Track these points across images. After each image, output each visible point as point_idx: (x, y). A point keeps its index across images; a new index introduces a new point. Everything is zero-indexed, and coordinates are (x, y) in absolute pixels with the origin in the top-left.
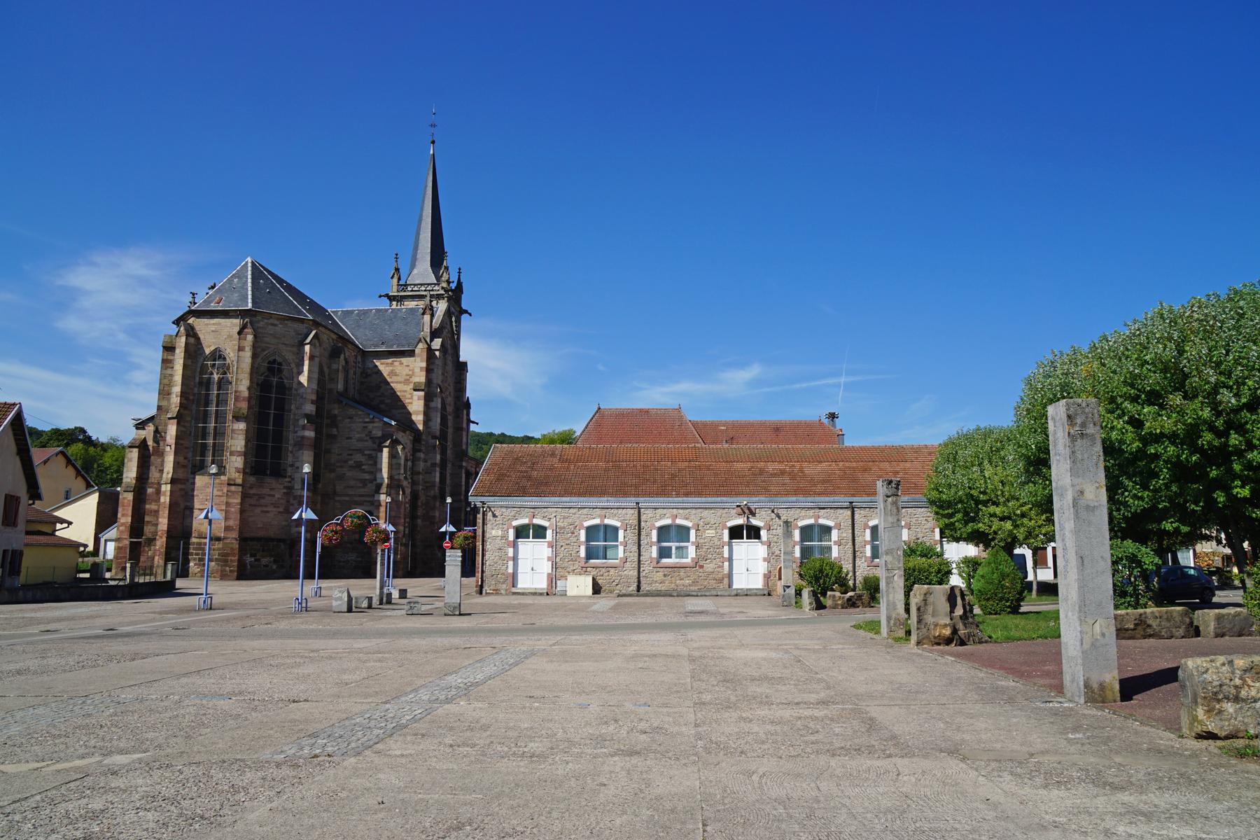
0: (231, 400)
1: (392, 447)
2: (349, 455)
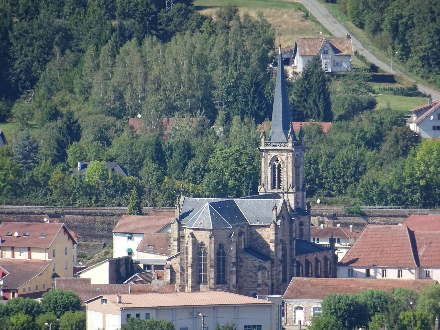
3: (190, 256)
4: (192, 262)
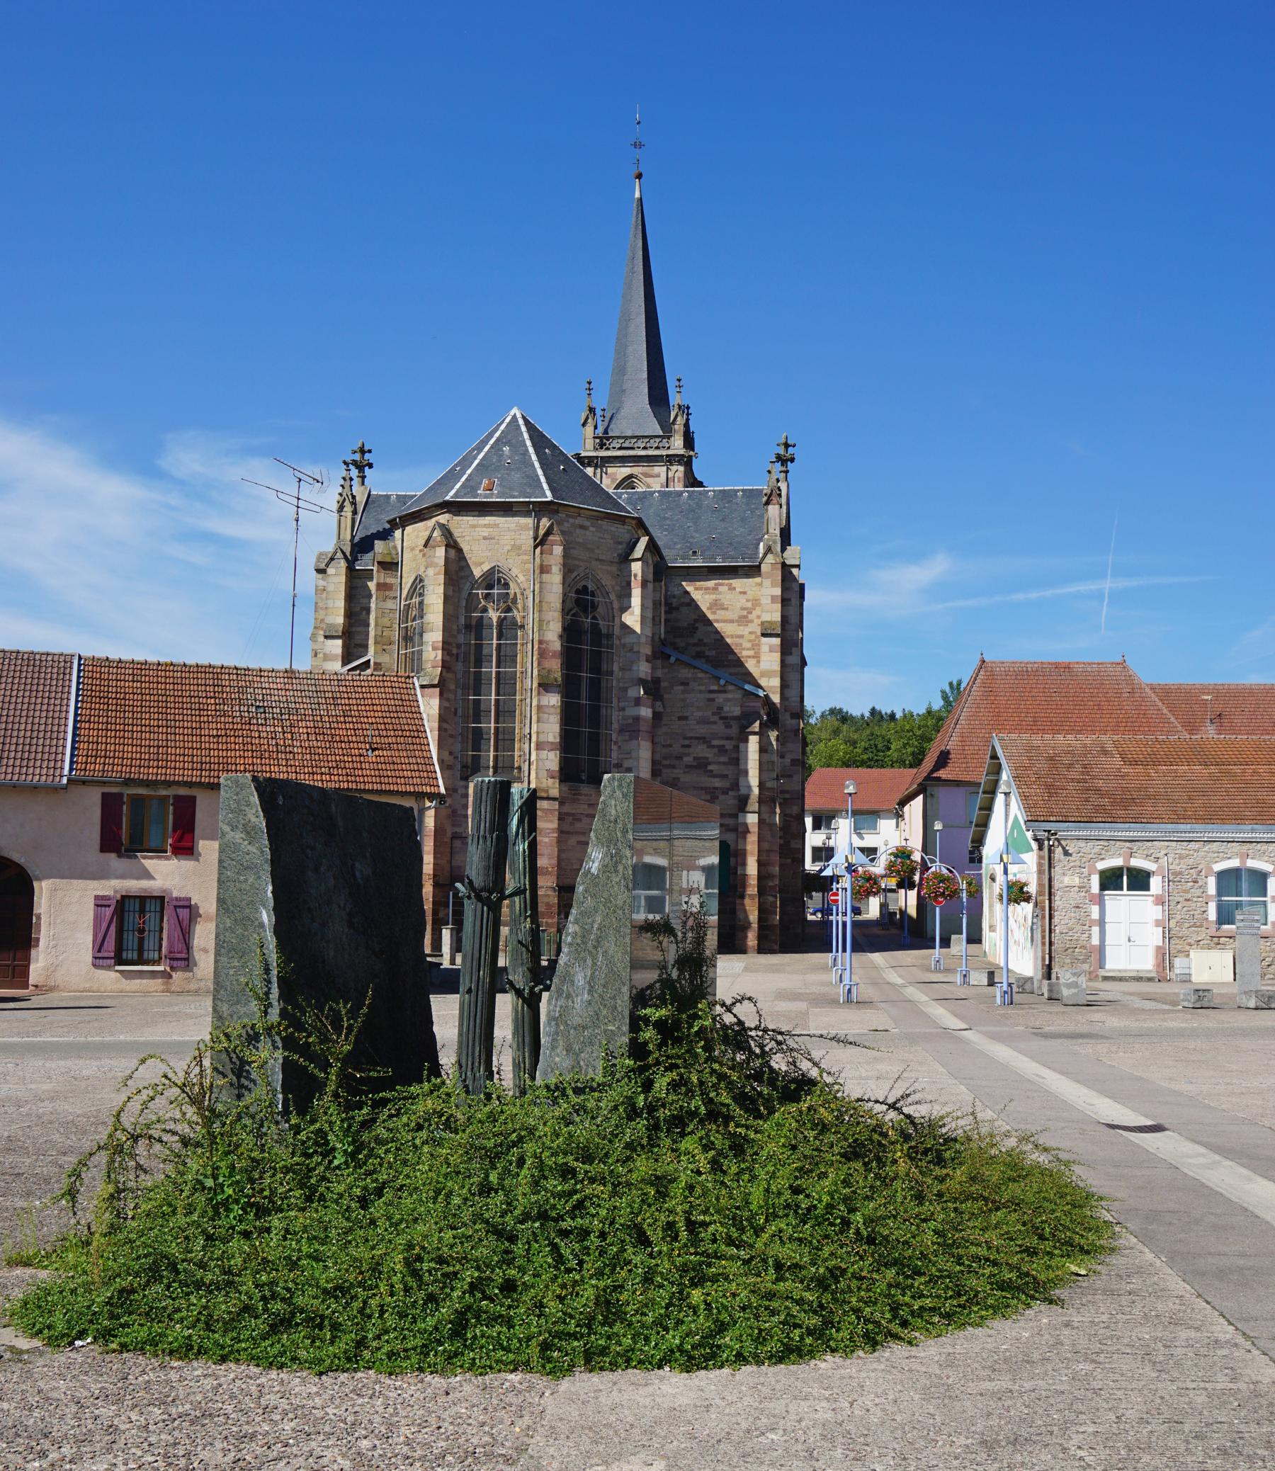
0: (525, 654)
1: (762, 734)
2: (683, 746)
3: (434, 637)
4: (445, 666)
